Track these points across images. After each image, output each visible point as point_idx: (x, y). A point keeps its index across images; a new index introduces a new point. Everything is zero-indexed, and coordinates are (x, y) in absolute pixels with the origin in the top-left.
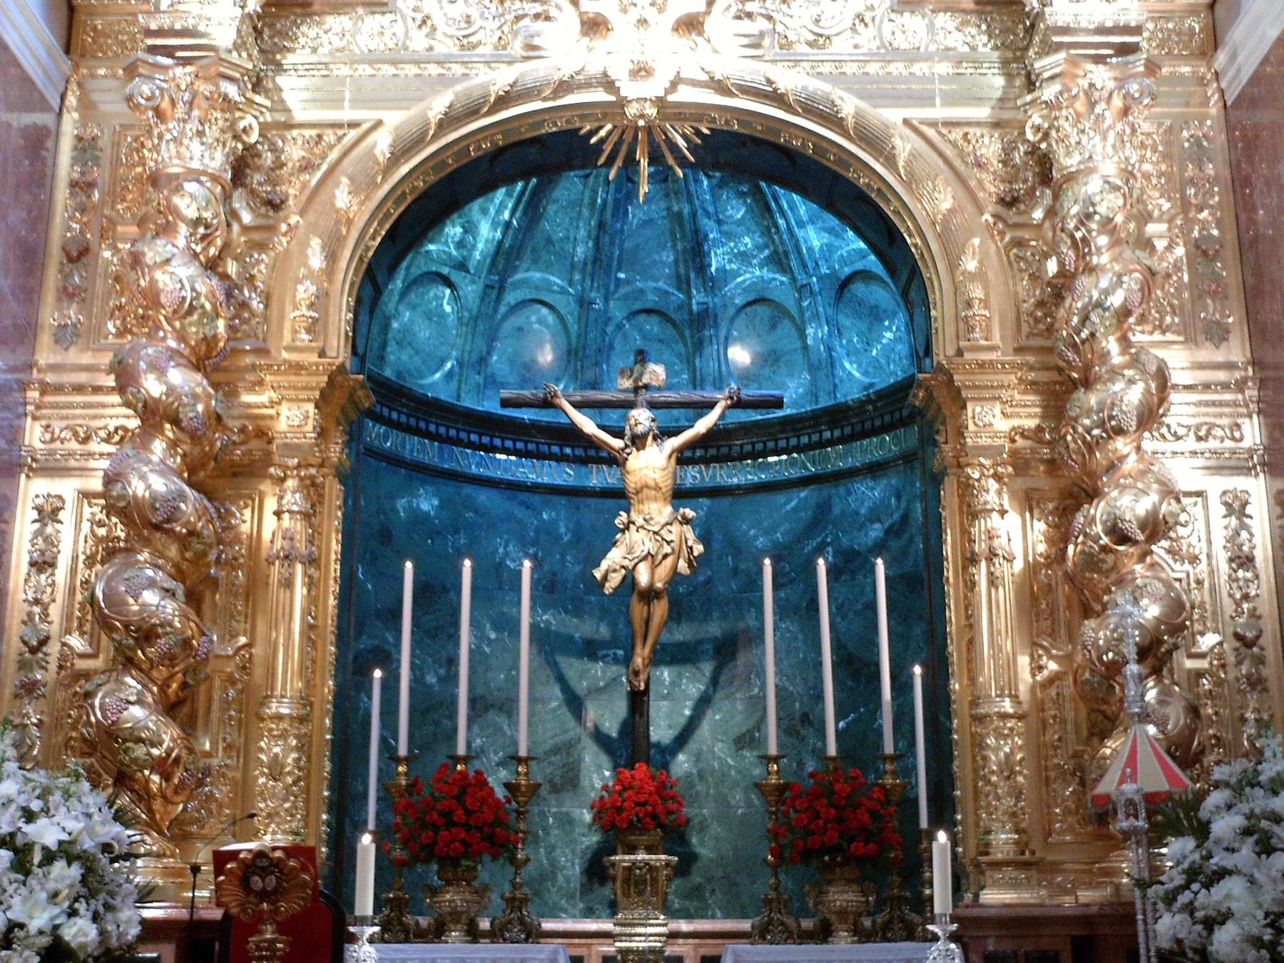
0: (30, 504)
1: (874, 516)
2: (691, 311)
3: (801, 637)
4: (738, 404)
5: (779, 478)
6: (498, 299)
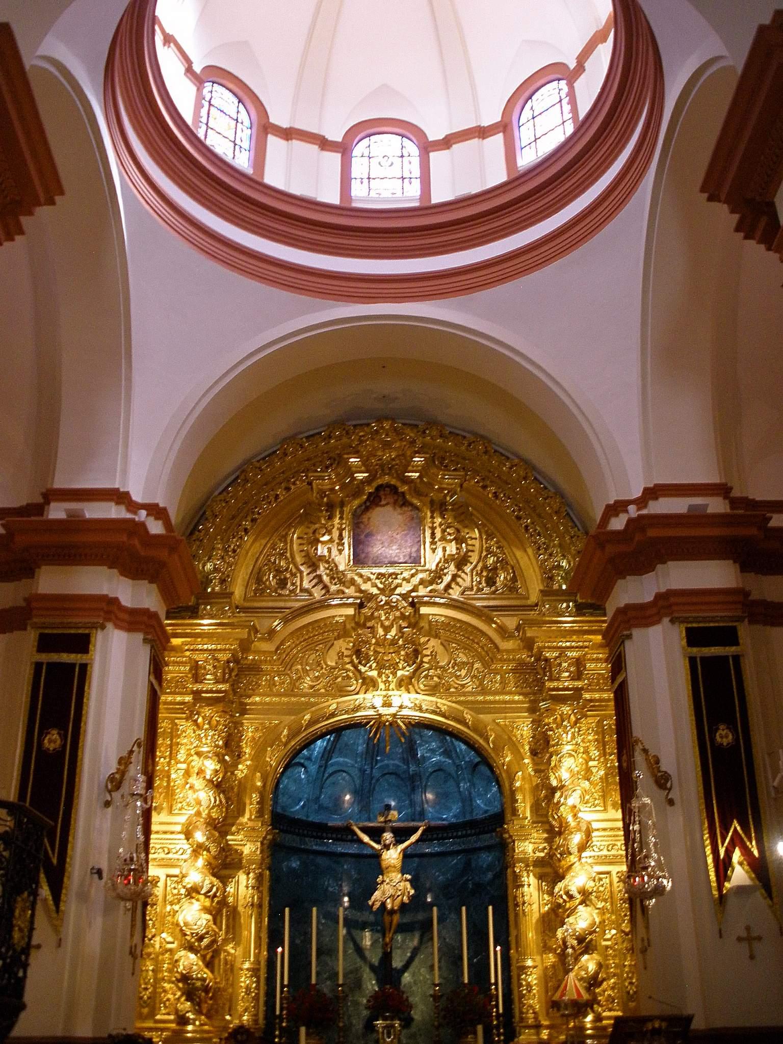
1: (490, 868)
6: (324, 772)
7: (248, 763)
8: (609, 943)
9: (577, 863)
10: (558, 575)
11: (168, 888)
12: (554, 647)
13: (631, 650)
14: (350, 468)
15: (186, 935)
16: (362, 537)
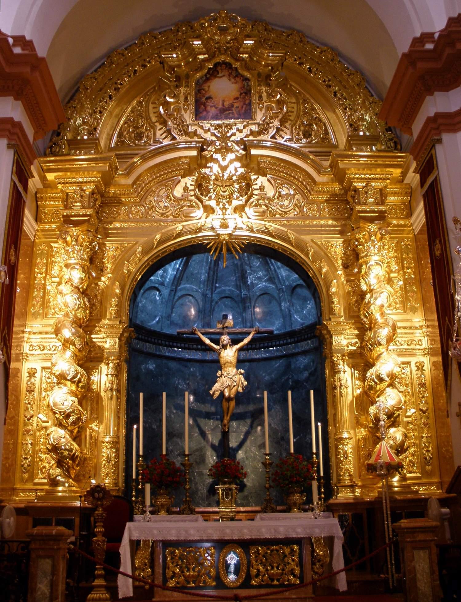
0: (26, 371)
1: (306, 368)
2: (241, 297)
3: (281, 410)
4: (258, 333)
5: (272, 355)
6: (174, 295)
7: (110, 275)
8: (410, 419)
9: (385, 353)
10: (363, 125)
11: (44, 378)
12: (361, 179)
13: (440, 152)
14: (193, 50)
15: (55, 413)
16: (204, 99)
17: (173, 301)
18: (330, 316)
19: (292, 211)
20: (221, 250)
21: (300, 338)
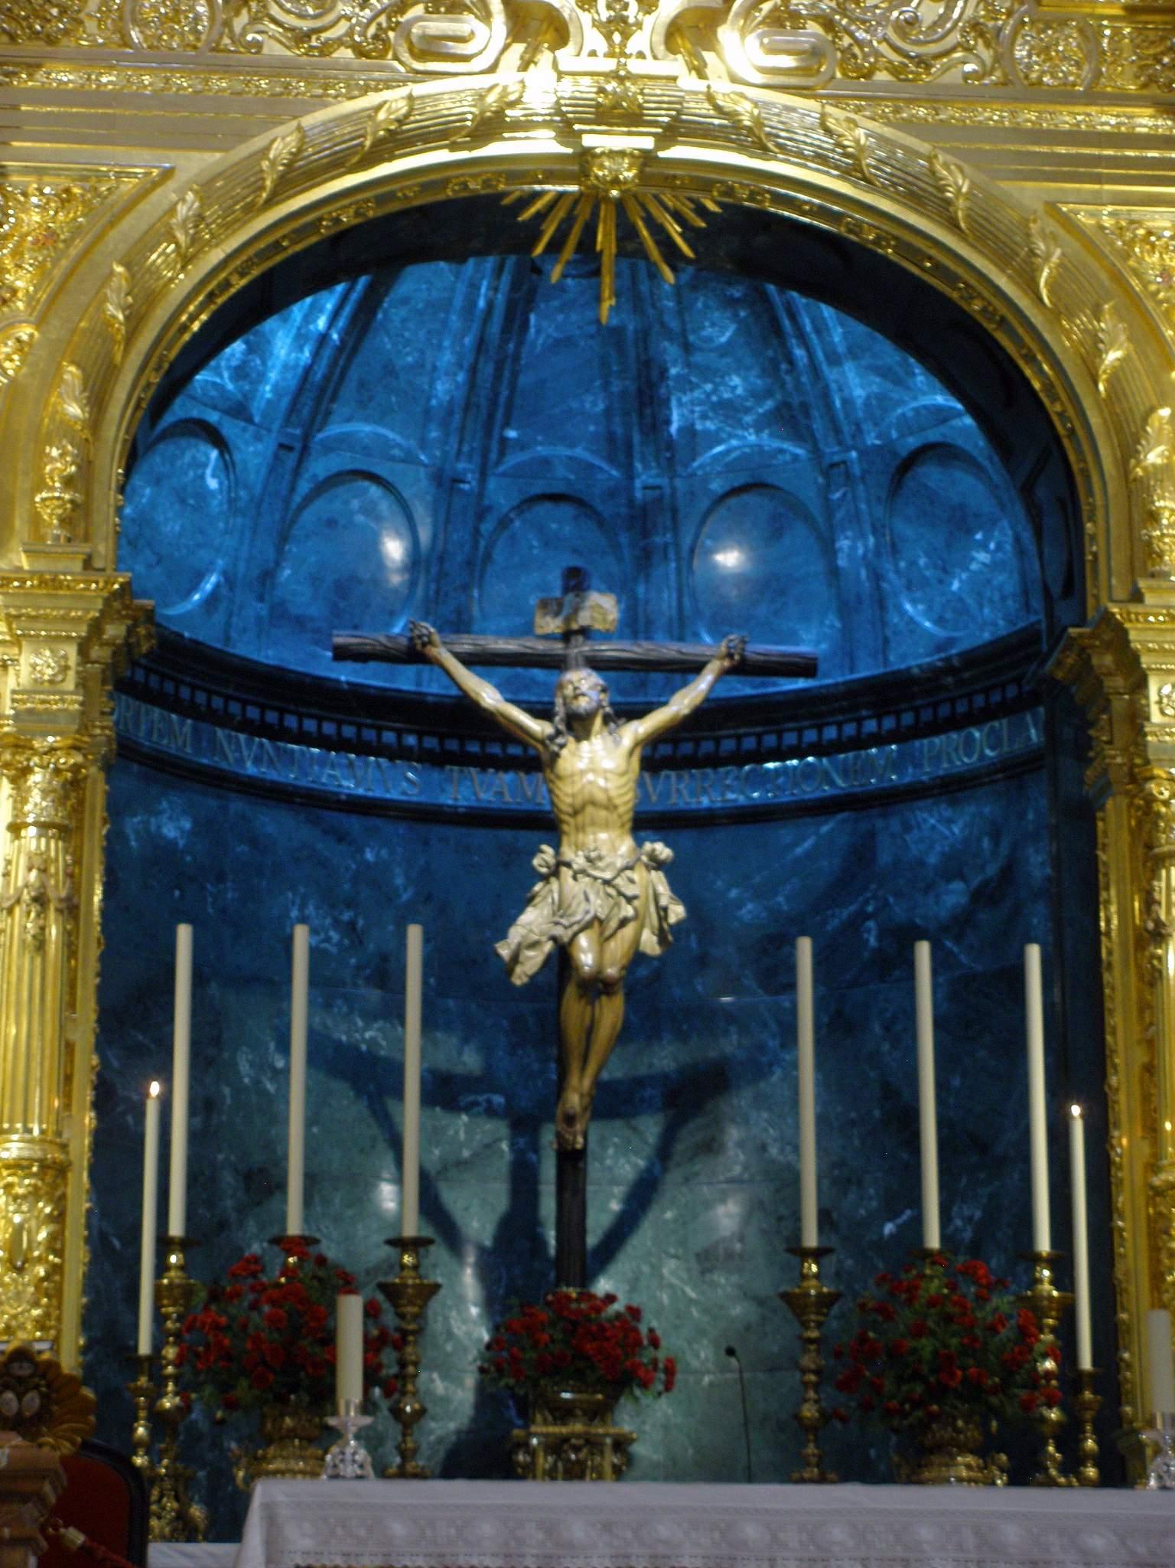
1: (953, 867)
2: (631, 502)
4: (741, 668)
5: (785, 798)
6: (297, 472)
7: (25, 332)
17: (287, 501)
18: (1142, 584)
19: (958, 55)
20: (590, 230)
21: (926, 715)
